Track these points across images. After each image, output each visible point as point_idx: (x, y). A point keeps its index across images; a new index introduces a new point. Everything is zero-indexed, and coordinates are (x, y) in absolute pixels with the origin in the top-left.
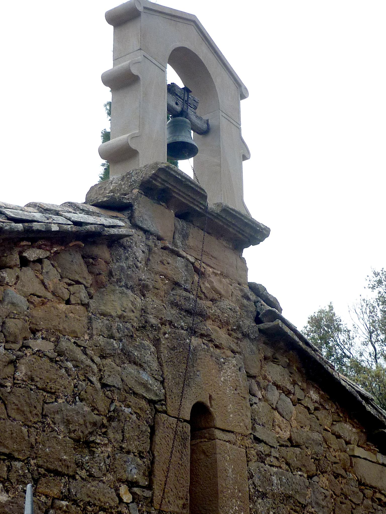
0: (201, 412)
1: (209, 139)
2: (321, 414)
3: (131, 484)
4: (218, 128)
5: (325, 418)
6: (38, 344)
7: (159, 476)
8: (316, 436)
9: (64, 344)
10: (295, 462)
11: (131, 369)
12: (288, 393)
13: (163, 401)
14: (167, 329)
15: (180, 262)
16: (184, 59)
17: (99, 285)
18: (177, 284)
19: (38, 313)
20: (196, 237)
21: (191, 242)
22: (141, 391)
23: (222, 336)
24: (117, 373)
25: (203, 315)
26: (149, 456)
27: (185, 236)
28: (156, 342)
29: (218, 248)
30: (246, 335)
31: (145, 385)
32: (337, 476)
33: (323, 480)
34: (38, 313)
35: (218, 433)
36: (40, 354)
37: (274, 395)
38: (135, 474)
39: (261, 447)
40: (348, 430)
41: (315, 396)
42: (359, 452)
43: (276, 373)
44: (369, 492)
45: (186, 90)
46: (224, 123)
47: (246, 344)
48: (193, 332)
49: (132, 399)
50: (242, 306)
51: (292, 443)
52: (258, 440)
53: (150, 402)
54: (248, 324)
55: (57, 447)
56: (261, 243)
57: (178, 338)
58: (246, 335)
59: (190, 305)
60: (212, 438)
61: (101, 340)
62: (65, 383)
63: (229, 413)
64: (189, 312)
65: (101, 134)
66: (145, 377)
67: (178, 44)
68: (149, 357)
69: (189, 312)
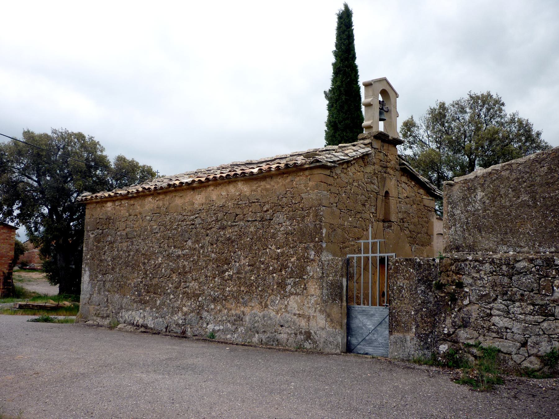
0: (387, 193)
1: (388, 113)
2: (414, 188)
3: (373, 213)
4: (391, 111)
5: (416, 189)
6: (355, 184)
7: (378, 210)
8: (413, 194)
9: (360, 183)
10: (408, 202)
11: (372, 185)
12: (406, 184)
13: (379, 192)
14: (379, 173)
15: (382, 154)
16: (384, 93)
17: (365, 165)
18: (381, 161)
19: (354, 176)
20: (386, 146)
21: (385, 148)
22: (374, 190)
23: (391, 172)
24: (370, 187)
25: (386, 167)
26: (376, 206)
27: (383, 147)
28: (377, 177)
29: (391, 148)
30: (397, 170)
31: (375, 189)
32: (418, 204)
33: (415, 206)
34: (354, 176)
35: (390, 198)
36: (355, 186)
37: (404, 185)
38: (373, 210)
39: (400, 200)
40: (421, 191)
41: (413, 183)
42: (424, 197)
43: (404, 179)
44: (426, 208)
45: (383, 101)
46: (393, 109)
47: (397, 172)
48: (385, 172)
49: (373, 193)
50: (396, 162)
51: (407, 197)
52: (399, 198)
53: (376, 193)
54: (398, 167)
55: (360, 208)
56: (333, 60)
57: (382, 175)
58: (397, 170)
59: (384, 166)
60: (389, 199)
61: (366, 180)
62: (360, 192)
63: (393, 193)
64: (384, 167)
65: (325, 124)
66: (375, 187)
67: (381, 89)
68: (376, 182)
69: (384, 167)
